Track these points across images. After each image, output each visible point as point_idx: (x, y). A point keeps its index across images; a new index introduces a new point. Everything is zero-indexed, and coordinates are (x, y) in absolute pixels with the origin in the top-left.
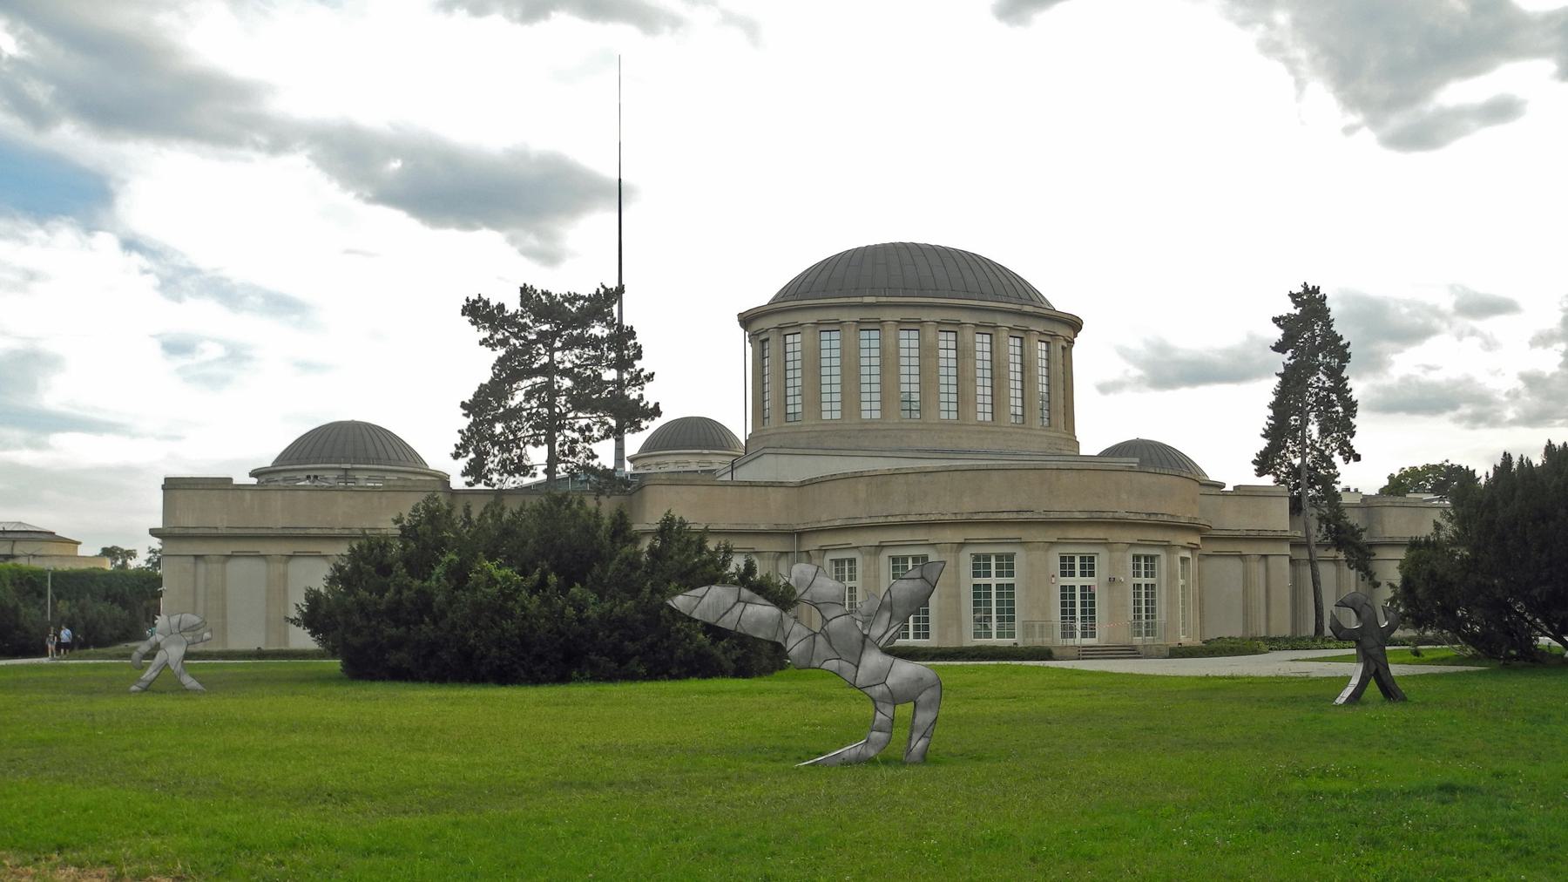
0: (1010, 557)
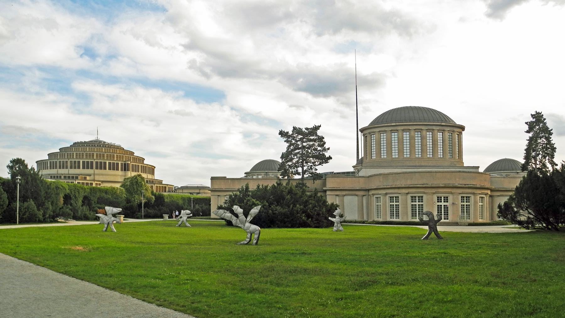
0: (422, 197)
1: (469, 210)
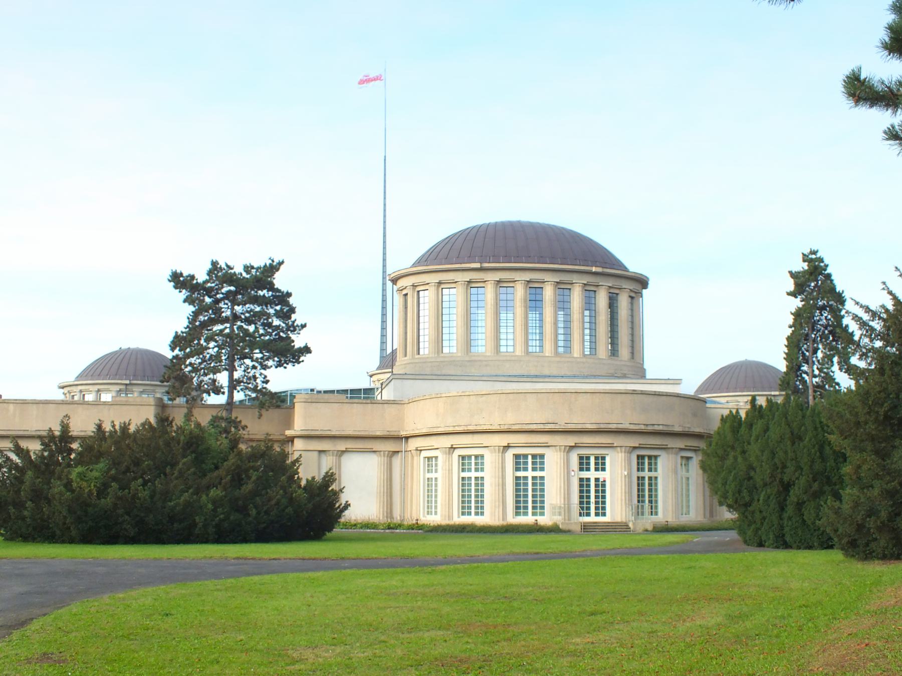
0: (542, 456)
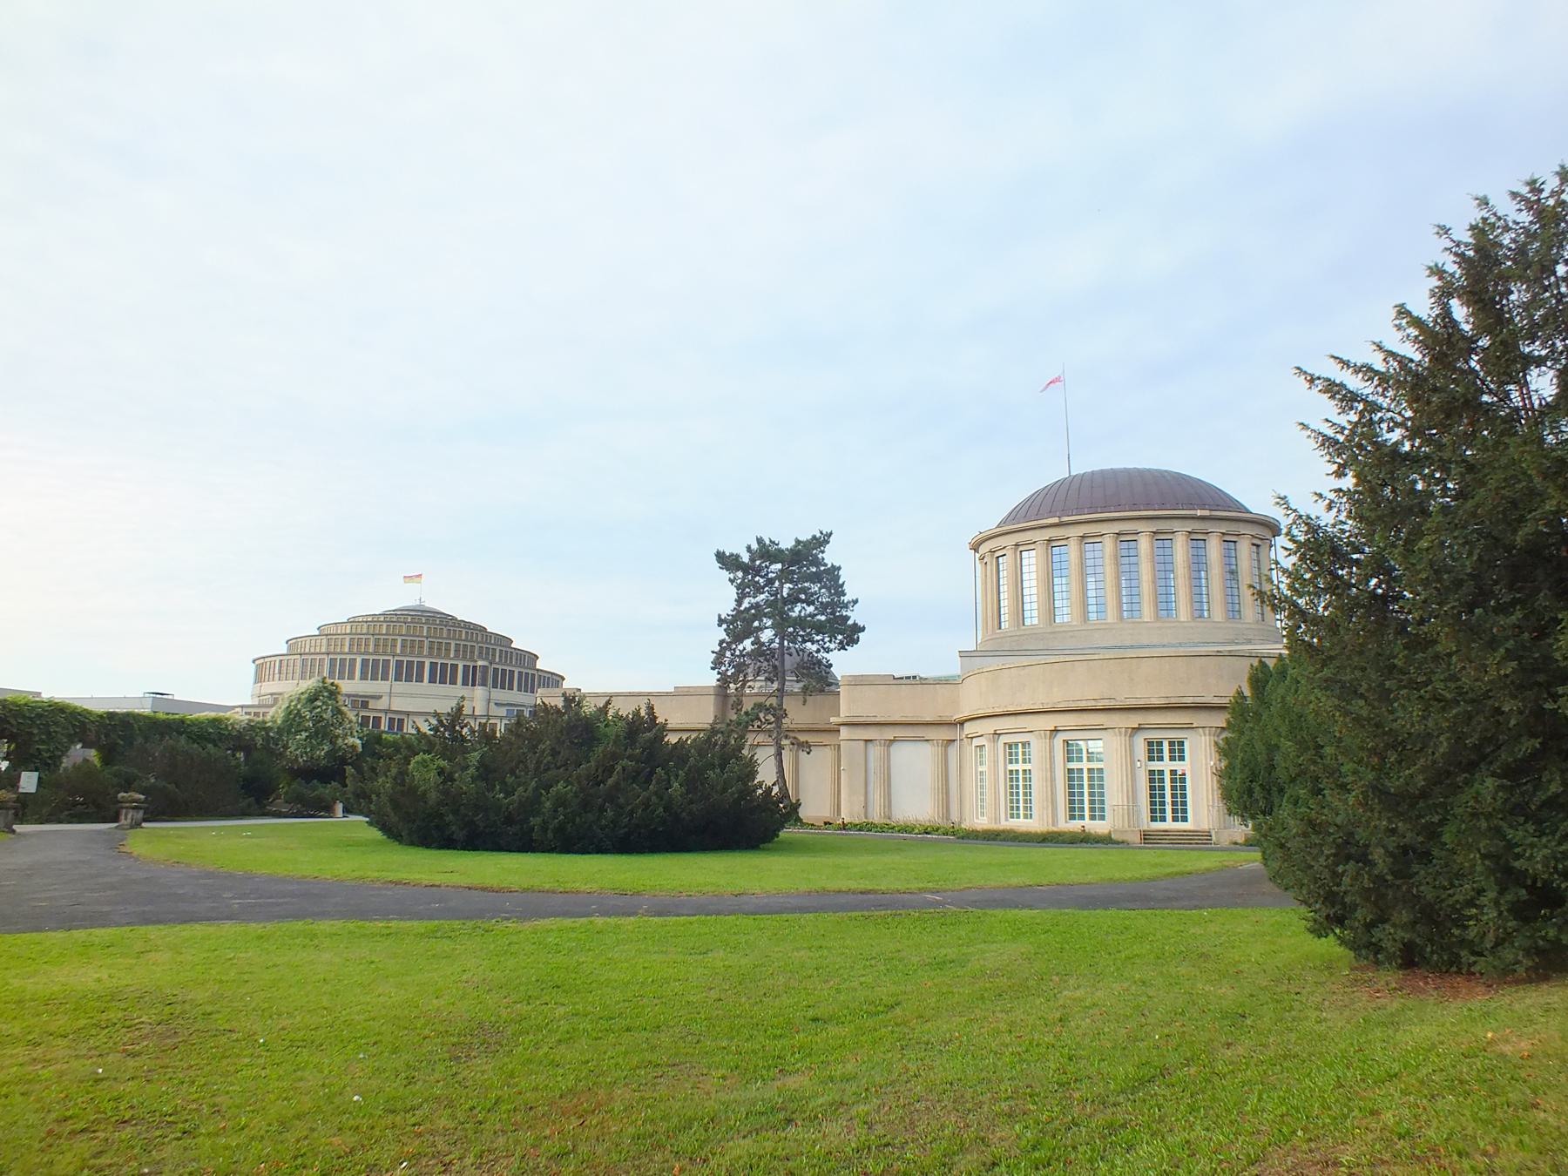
1: (1101, 787)
